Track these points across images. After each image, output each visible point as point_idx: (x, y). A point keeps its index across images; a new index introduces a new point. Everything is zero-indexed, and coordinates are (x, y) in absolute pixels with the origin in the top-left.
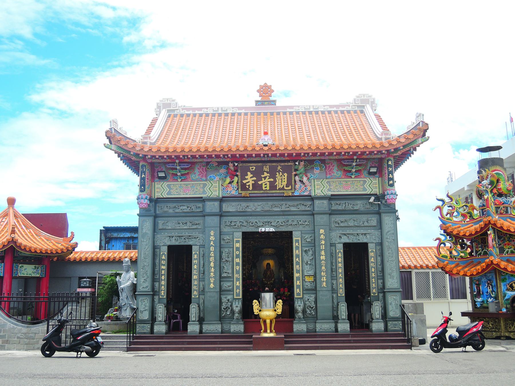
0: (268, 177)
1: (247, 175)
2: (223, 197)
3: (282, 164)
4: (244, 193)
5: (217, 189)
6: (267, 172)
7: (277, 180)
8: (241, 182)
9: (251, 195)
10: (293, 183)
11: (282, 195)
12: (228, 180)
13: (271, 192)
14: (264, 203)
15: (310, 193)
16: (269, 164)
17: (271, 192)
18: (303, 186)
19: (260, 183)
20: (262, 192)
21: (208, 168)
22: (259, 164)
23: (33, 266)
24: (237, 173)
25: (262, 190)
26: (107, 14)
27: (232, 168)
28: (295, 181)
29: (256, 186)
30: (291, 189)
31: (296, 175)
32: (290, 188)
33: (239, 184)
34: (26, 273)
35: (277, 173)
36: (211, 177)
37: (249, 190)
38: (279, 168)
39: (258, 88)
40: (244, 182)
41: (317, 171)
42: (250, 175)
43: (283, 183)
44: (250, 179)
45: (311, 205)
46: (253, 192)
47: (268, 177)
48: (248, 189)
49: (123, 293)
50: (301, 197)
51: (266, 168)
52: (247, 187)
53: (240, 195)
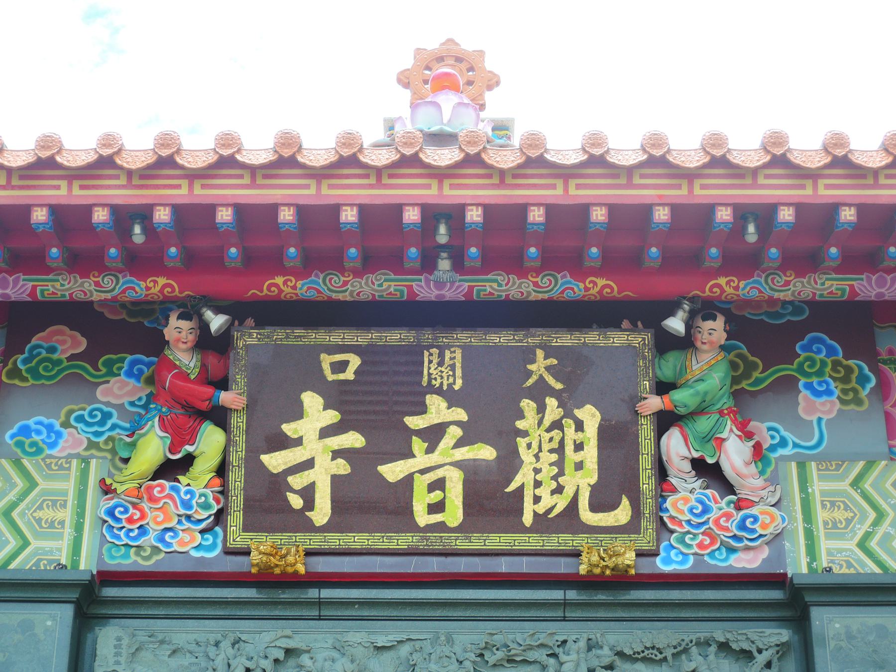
0: (455, 432)
1: (297, 413)
2: (108, 578)
3: (565, 339)
4: (263, 548)
5: (67, 515)
6: (452, 398)
7: (527, 456)
8: (254, 468)
9: (323, 565)
10: (647, 483)
11: (562, 566)
12: (153, 447)
13: (477, 542)
14: (421, 631)
15: (779, 555)
16: (464, 337)
17: (477, 542)
18: (721, 505)
19: (393, 471)
20: (403, 541)
21: (15, 373)
22: (395, 337)
24: (225, 398)
25: (411, 526)
27: (187, 361)
28: (662, 471)
29: (367, 501)
30: (633, 527)
31: (666, 421)
32: (622, 514)
33: (237, 478)
35: (528, 405)
36: (25, 431)
37: (310, 527)
38: (539, 366)
39: (408, 62)
40: (275, 461)
41: (818, 407)
42: (316, 414)
43: (570, 481)
44: (315, 447)
45: (783, 649)
46: (335, 540)
47: (455, 432)
48: (300, 522)
50: (709, 590)
51: (445, 364)
52: (296, 502)
53: (233, 565)
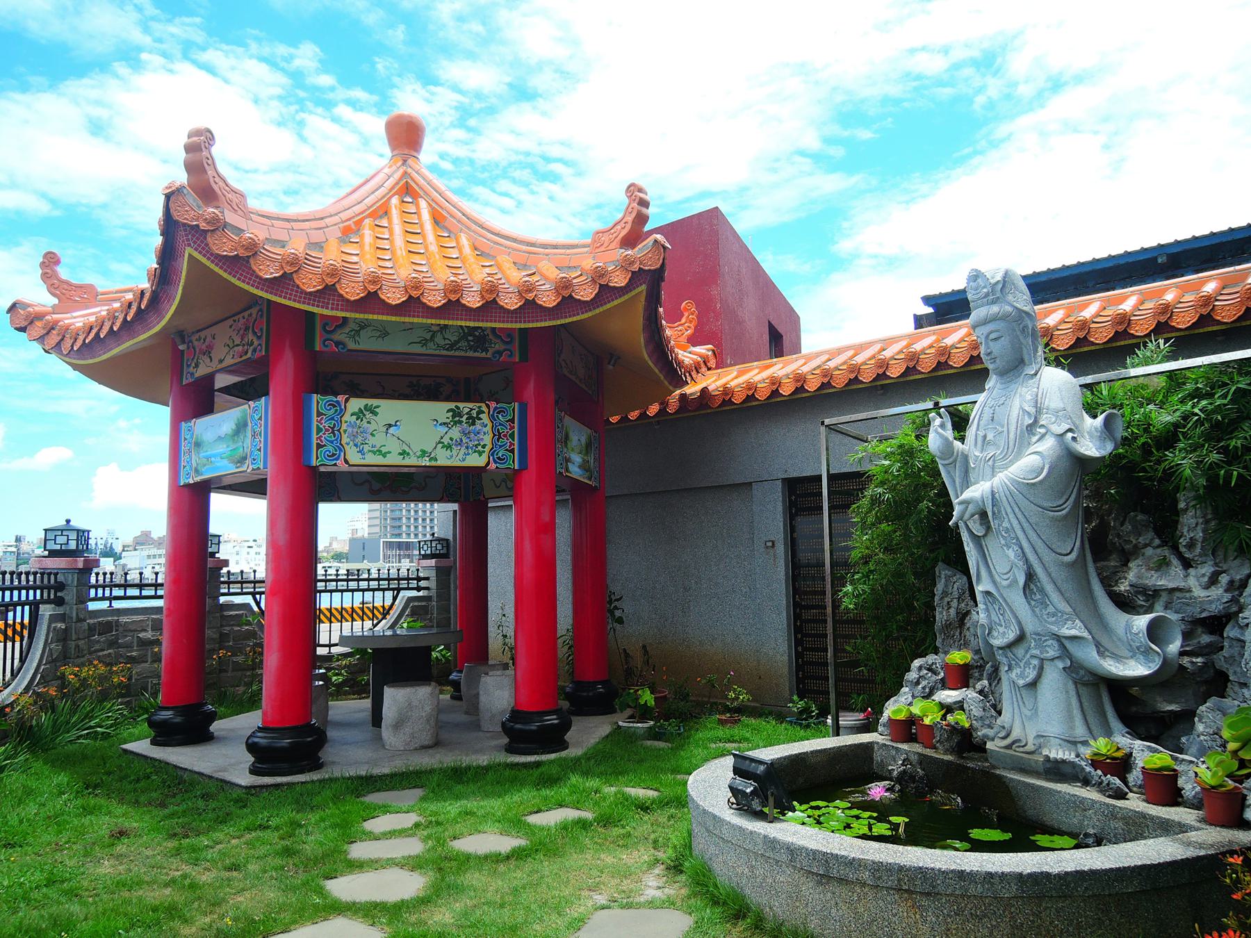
23: (441, 409)
26: (933, 65)
34: (393, 447)
49: (991, 544)
